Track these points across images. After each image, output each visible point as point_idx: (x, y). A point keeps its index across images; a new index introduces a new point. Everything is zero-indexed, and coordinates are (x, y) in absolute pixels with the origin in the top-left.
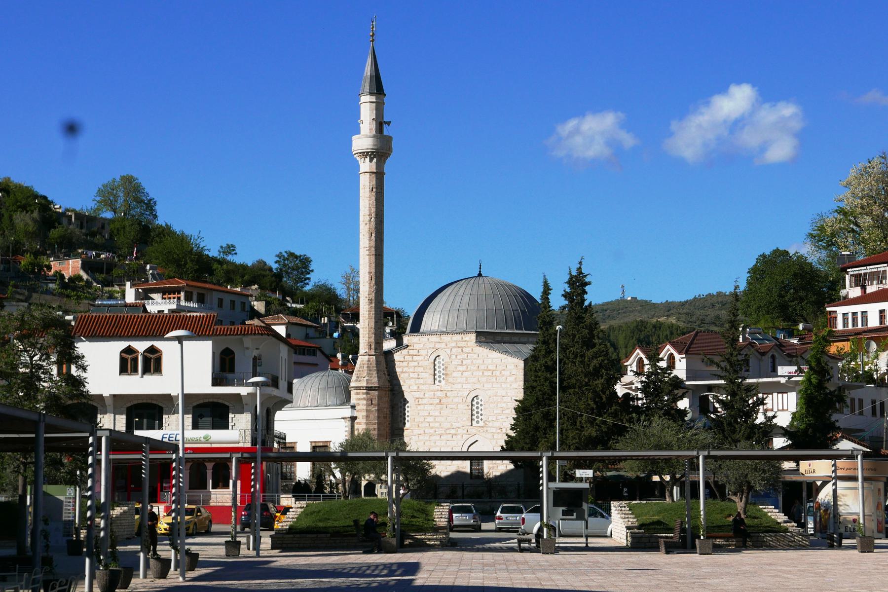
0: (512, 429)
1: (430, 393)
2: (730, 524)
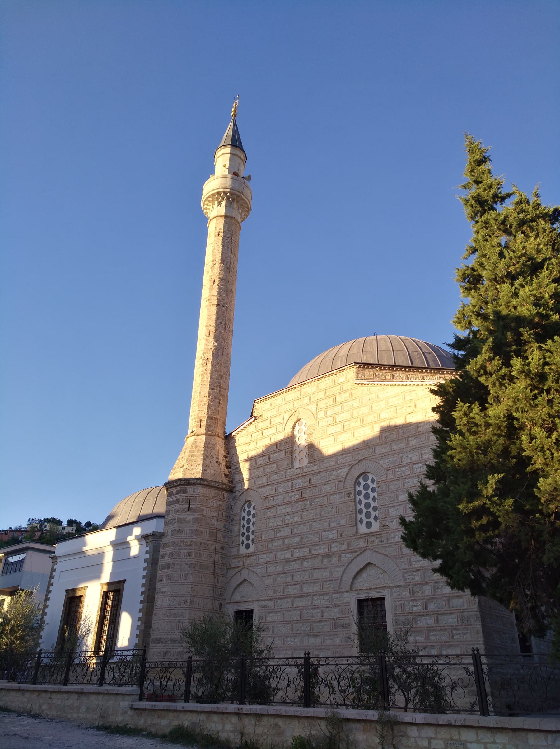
0: (429, 475)
1: (286, 484)
2: (392, 709)
